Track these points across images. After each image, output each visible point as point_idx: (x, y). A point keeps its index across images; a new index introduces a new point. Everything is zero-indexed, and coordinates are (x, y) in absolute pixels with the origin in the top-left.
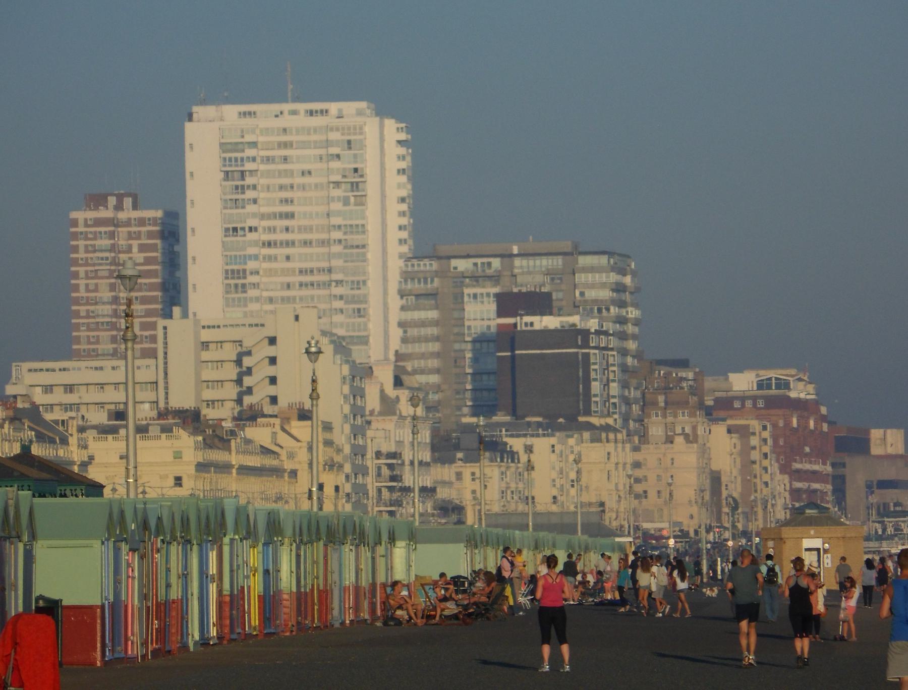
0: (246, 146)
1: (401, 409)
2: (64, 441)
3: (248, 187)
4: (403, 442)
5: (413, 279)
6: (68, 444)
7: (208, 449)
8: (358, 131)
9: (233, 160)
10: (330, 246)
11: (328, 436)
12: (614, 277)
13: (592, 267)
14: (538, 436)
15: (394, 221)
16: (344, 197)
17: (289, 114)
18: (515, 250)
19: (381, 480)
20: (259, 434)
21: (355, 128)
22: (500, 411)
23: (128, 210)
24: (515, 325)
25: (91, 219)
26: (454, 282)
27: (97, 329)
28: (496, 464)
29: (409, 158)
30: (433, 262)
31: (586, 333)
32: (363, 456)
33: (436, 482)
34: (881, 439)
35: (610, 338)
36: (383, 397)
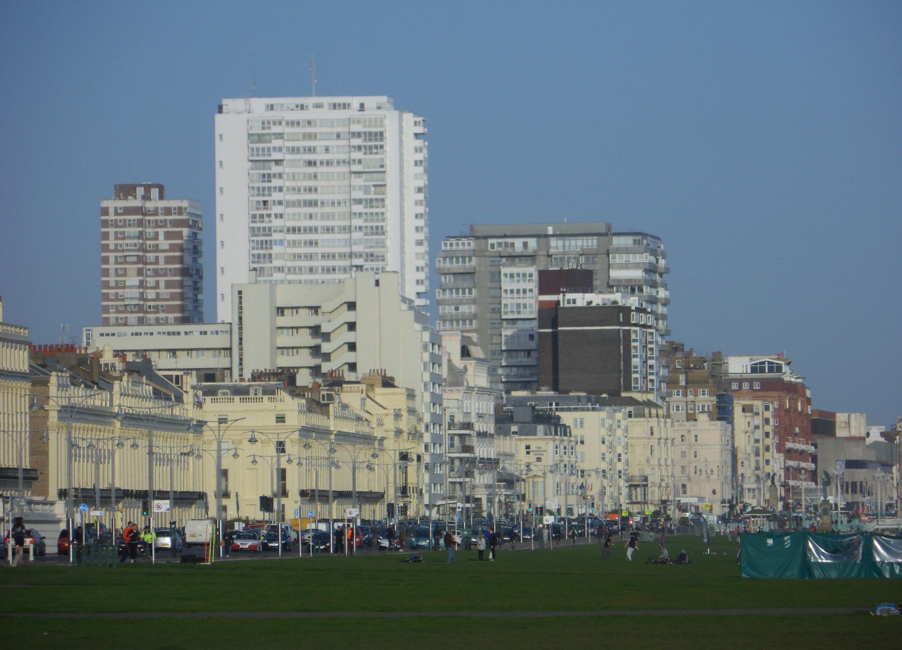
0: (273, 137)
1: (469, 380)
2: (179, 399)
3: (275, 175)
4: (470, 413)
5: (451, 258)
6: (183, 402)
8: (373, 124)
9: (255, 150)
10: (351, 232)
12: (647, 258)
13: (627, 248)
14: (588, 410)
15: (412, 209)
16: (365, 186)
17: (323, 104)
18: (550, 231)
19: (455, 451)
20: (351, 397)
21: (370, 121)
22: (543, 386)
23: (155, 200)
24: (558, 302)
25: (120, 208)
26: (492, 261)
27: (125, 312)
28: (551, 437)
29: (425, 151)
30: (471, 242)
31: (627, 310)
32: (440, 425)
33: (499, 454)
34: (845, 422)
35: (648, 315)
36: (451, 367)
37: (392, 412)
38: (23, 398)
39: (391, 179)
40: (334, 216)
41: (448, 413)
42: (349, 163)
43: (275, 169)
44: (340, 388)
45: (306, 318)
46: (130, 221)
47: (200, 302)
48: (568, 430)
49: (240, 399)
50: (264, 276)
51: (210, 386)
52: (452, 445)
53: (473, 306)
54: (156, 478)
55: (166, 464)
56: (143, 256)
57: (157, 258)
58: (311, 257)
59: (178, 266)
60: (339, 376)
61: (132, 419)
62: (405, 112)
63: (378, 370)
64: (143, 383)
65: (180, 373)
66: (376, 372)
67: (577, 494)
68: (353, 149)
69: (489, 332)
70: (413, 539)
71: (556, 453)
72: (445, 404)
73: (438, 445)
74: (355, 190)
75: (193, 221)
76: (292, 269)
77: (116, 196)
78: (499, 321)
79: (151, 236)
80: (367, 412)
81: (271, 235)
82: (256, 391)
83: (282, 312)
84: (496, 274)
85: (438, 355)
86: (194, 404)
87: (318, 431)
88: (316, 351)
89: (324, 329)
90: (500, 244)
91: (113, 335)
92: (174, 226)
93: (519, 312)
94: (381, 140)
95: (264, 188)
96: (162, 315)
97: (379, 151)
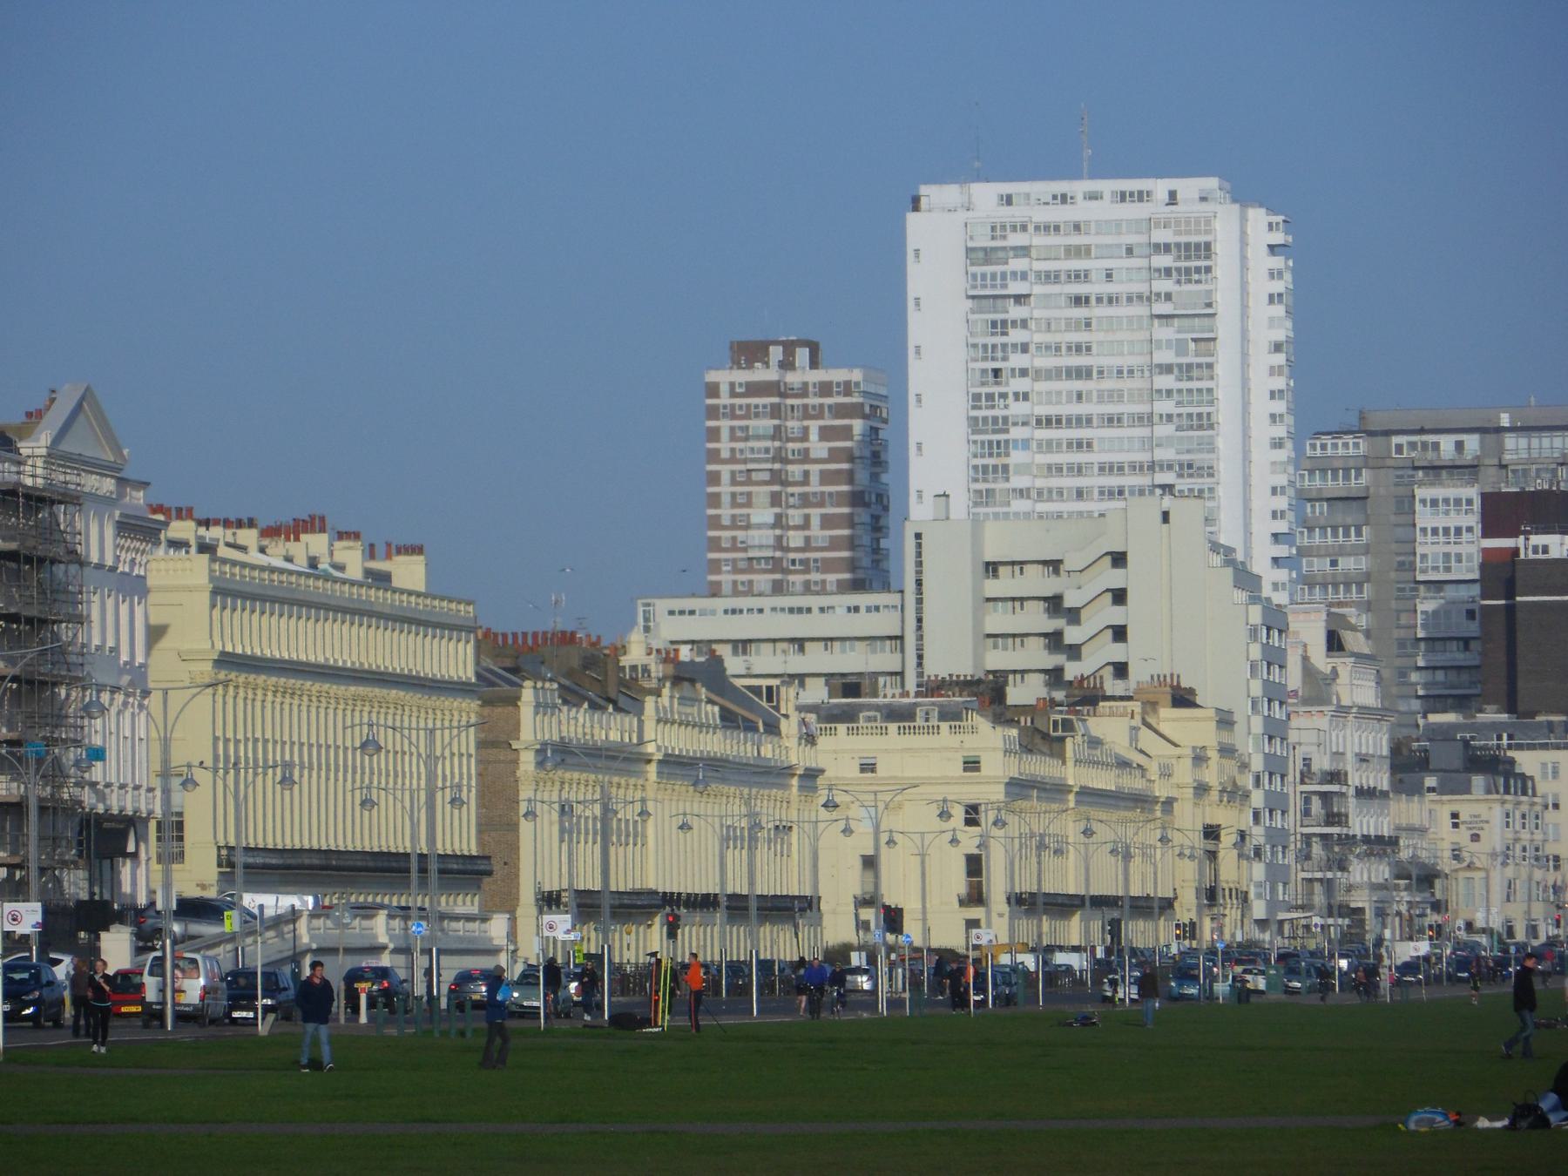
0: (1011, 254)
2: (773, 729)
3: (1014, 323)
4: (1343, 754)
5: (1324, 471)
7: (1027, 753)
11: (1226, 738)
18: (1505, 420)
20: (1111, 727)
22: (1489, 704)
24: (1516, 551)
26: (1398, 477)
27: (750, 570)
29: (1288, 276)
30: (1361, 441)
32: (1283, 777)
33: (1398, 828)
37: (1189, 752)
38: (349, 731)
39: (1226, 328)
40: (1121, 396)
41: (1300, 752)
42: (1149, 299)
43: (1015, 312)
44: (1091, 708)
45: (1037, 582)
46: (757, 406)
47: (885, 552)
48: (1530, 784)
49: (899, 728)
50: (995, 505)
51: (848, 705)
52: (1307, 813)
53: (1364, 558)
54: (1046, 877)
55: (732, 846)
56: (780, 471)
57: (806, 474)
58: (1080, 470)
59: (845, 488)
60: (1095, 687)
61: (674, 765)
62: (1252, 206)
63: (1165, 676)
64: (701, 701)
65: (774, 682)
66: (1156, 678)
67: (1546, 900)
68: (1157, 275)
69: (1393, 604)
70: (1173, 984)
71: (1508, 826)
72: (1293, 737)
73: (1279, 812)
74: (1159, 348)
75: (871, 406)
76: (1045, 492)
77: (733, 362)
78: (1413, 585)
79: (796, 435)
80: (1142, 751)
81: (1007, 431)
82: (927, 713)
83: (995, 571)
84: (1406, 500)
85: (1280, 647)
86: (800, 738)
87: (1043, 786)
88: (1054, 641)
89: (1068, 603)
90: (1413, 445)
91: (692, 613)
92: (837, 417)
93: (1448, 569)
94: (1208, 257)
95: (994, 347)
96: (815, 576)
97: (1203, 277)
